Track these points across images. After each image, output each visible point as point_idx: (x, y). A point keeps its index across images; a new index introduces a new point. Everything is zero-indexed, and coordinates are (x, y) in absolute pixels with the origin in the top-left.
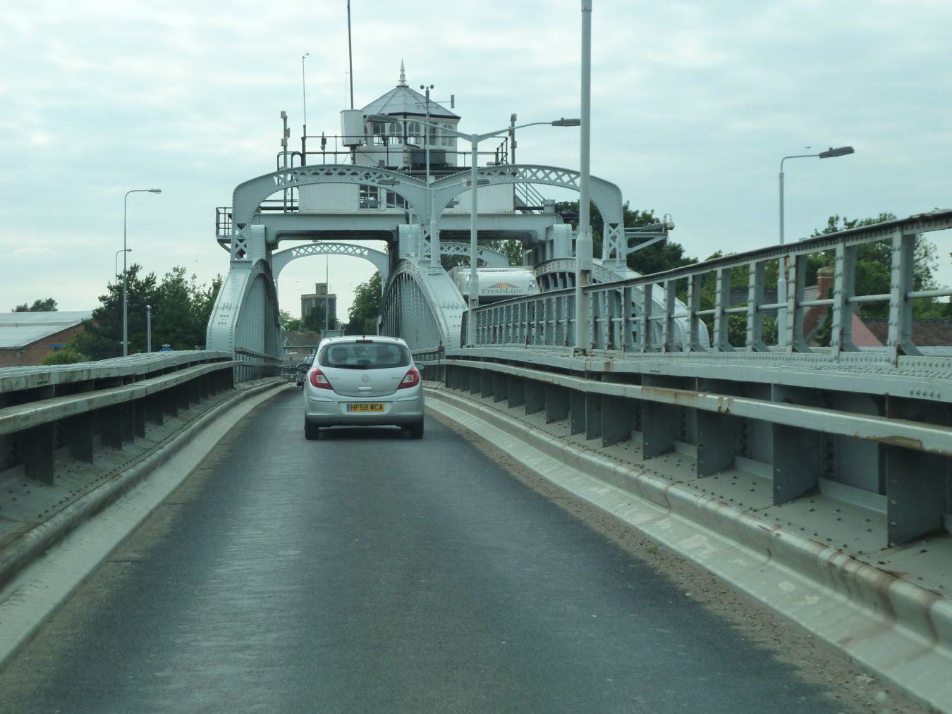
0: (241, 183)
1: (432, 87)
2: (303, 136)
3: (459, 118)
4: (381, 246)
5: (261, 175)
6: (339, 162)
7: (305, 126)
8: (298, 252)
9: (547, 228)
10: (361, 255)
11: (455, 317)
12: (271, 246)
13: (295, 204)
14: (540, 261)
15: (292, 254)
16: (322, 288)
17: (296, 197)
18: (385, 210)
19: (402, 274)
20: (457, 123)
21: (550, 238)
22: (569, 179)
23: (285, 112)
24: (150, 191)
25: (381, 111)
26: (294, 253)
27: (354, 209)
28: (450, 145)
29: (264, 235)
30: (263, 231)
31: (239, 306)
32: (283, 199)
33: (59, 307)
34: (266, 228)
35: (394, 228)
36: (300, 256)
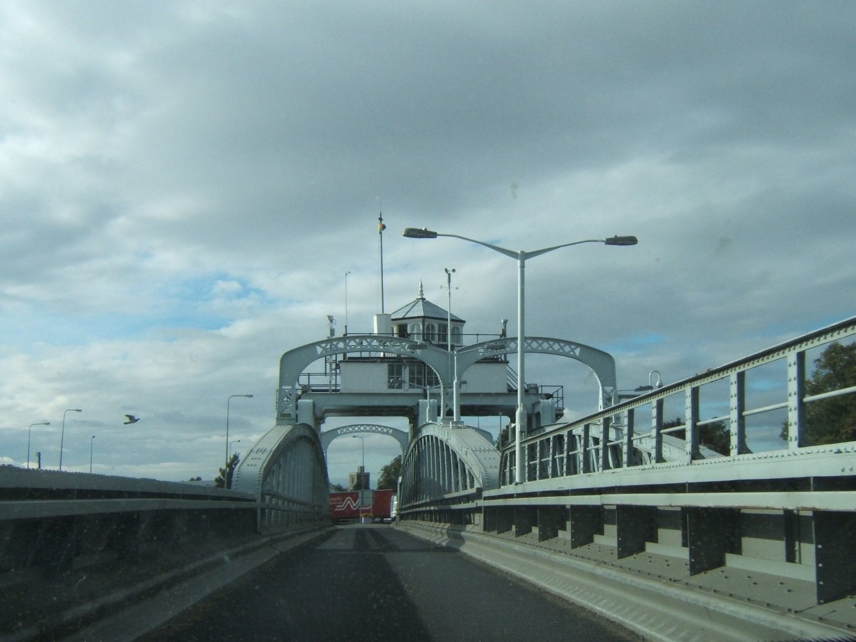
0: (288, 351)
1: (454, 271)
2: (345, 333)
3: (464, 322)
4: (402, 423)
5: (303, 344)
6: (372, 356)
7: (346, 327)
8: (342, 431)
9: (533, 404)
10: (387, 433)
11: (490, 459)
12: (320, 420)
13: (338, 388)
14: (534, 426)
15: (338, 432)
16: (362, 468)
17: (339, 382)
18: (408, 390)
19: (424, 437)
20: (463, 326)
21: (536, 411)
22: (570, 349)
23: (332, 316)
24: (246, 396)
25: (405, 316)
26: (339, 432)
27: (383, 387)
28: (457, 342)
29: (312, 408)
30: (312, 405)
31: (273, 450)
32: (324, 372)
33: (202, 480)
34: (314, 405)
35: (415, 404)
36: (343, 434)
